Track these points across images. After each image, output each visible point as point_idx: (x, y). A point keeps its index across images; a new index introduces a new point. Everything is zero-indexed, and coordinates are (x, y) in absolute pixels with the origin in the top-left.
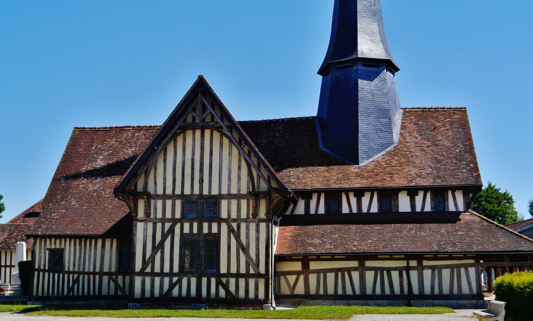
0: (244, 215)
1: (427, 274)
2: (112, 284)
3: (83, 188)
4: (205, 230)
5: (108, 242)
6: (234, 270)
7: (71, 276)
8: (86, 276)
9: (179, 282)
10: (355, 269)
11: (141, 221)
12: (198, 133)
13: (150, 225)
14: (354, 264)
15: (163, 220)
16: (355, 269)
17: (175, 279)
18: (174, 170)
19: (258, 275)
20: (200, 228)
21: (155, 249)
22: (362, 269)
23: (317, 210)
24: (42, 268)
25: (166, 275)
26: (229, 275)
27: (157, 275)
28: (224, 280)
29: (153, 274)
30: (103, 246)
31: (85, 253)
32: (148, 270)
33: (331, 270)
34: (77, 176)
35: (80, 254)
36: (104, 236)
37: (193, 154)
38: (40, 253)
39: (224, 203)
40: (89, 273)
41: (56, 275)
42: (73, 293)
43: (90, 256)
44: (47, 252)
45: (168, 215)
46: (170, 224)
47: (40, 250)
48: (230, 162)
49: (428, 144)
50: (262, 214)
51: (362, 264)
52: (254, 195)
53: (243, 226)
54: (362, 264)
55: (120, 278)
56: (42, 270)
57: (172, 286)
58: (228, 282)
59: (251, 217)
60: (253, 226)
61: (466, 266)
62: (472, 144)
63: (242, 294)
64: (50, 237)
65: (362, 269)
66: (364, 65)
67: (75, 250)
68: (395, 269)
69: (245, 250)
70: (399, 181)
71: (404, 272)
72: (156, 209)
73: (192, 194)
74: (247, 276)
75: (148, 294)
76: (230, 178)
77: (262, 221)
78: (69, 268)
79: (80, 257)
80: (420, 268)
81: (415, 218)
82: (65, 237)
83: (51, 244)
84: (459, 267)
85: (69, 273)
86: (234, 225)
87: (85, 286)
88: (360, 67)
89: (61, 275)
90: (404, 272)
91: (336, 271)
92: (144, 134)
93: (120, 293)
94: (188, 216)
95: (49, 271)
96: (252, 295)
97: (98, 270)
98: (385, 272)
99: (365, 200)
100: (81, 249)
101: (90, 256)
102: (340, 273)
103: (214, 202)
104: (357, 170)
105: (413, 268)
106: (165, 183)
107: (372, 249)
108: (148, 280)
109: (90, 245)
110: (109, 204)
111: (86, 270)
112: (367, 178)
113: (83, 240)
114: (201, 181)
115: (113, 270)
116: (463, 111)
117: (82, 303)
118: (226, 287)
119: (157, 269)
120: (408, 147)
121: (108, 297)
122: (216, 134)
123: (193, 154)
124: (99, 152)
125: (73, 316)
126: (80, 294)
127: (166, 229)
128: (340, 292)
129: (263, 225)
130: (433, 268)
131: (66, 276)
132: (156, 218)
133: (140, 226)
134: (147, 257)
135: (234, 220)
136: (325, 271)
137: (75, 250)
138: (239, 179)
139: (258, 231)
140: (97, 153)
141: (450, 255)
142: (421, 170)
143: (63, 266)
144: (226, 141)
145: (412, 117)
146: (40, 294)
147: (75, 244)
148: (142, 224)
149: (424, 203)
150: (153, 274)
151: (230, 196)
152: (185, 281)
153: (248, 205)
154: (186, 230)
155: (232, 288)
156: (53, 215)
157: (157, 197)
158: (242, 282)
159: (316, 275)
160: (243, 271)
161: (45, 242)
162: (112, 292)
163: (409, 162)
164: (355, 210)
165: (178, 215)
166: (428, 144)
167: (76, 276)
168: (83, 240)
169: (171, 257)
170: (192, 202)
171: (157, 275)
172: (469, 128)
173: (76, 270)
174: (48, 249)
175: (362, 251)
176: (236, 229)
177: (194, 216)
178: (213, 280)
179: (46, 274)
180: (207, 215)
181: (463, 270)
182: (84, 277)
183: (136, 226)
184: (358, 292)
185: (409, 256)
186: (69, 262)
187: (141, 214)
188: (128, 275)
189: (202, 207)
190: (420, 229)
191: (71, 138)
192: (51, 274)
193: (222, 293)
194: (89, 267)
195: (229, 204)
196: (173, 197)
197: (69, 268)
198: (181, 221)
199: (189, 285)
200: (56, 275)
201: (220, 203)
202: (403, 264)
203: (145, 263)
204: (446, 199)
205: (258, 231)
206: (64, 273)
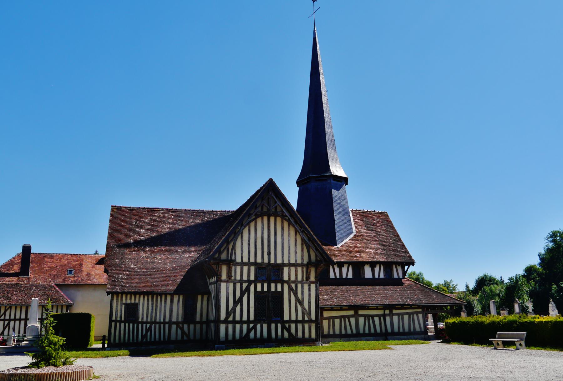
0: (299, 278)
1: (395, 318)
3: (136, 254)
4: (273, 289)
6: (293, 318)
7: (144, 325)
8: (157, 326)
9: (255, 327)
10: (352, 316)
11: (224, 282)
12: (266, 219)
13: (231, 285)
14: (352, 313)
15: (242, 281)
16: (352, 316)
17: (251, 325)
18: (249, 244)
19: (310, 321)
20: (269, 287)
21: (236, 303)
22: (356, 316)
23: (379, 276)
24: (119, 319)
25: (245, 322)
26: (290, 321)
27: (238, 322)
28: (287, 325)
29: (234, 322)
30: (172, 301)
31: (156, 307)
32: (231, 319)
33: (337, 317)
34: (128, 245)
35: (152, 307)
36: (172, 295)
37: (263, 234)
38: (117, 307)
39: (286, 270)
40: (160, 323)
41: (131, 325)
42: (147, 339)
43: (160, 309)
44: (123, 306)
45: (245, 278)
46: (247, 284)
47: (117, 304)
48: (289, 240)
49: (374, 234)
50: (312, 278)
51: (356, 313)
52: (308, 266)
53: (299, 286)
54: (356, 313)
55: (186, 326)
56: (118, 321)
57: (249, 331)
58: (290, 326)
59: (305, 279)
60: (306, 286)
62: (398, 235)
63: (300, 335)
64: (131, 293)
65: (356, 316)
66: (334, 180)
67: (148, 304)
68: (376, 316)
69: (301, 303)
70: (366, 258)
71: (382, 318)
72: (235, 272)
73: (263, 262)
74: (303, 322)
75: (230, 337)
76: (289, 252)
77: (312, 282)
78: (143, 319)
79: (152, 309)
80: (391, 315)
81: (374, 282)
82: (140, 294)
83: (126, 300)
84: (413, 313)
85: (142, 323)
86: (293, 285)
87: (156, 333)
88: (332, 181)
89: (136, 325)
90: (382, 318)
91: (340, 317)
92: (173, 215)
93: (185, 338)
94: (259, 279)
95: (125, 322)
96: (307, 335)
97: (167, 320)
98: (370, 318)
99: (344, 270)
100: (153, 304)
101: (160, 309)
102: (343, 319)
103: (279, 268)
104: (337, 249)
105: (388, 315)
106: (242, 254)
107: (365, 303)
108: (230, 327)
109: (161, 300)
110: (164, 268)
111: (158, 320)
112: (346, 255)
113: (155, 296)
114: (269, 254)
115: (180, 319)
116: (113, 208)
117: (155, 347)
118: (289, 330)
119: (238, 318)
120: (362, 235)
121: (176, 342)
122: (279, 220)
123: (263, 234)
124: (140, 227)
125: (203, 356)
126: (153, 340)
127: (244, 288)
128: (343, 332)
129: (313, 286)
130: (398, 315)
131: (140, 326)
132: (235, 279)
133: (223, 285)
134: (230, 309)
135: (293, 282)
136: (334, 318)
138: (296, 253)
139: (309, 290)
140: (138, 228)
141: (411, 306)
142: (372, 252)
144: (286, 224)
145: (358, 216)
147: (148, 299)
148: (225, 284)
149: (380, 273)
151: (290, 265)
152: (259, 326)
153: (303, 272)
154: (259, 288)
155: (293, 331)
156: (120, 276)
157: (238, 264)
158: (300, 326)
159: (327, 321)
160: (300, 318)
162: (179, 337)
163: (368, 246)
164: (338, 277)
165: (252, 278)
166: (374, 234)
167: (148, 325)
168: (155, 296)
169: (248, 309)
170: (263, 268)
171: (238, 322)
172: (393, 225)
173: (149, 320)
174: (124, 304)
175: (359, 304)
176: (294, 288)
177: (264, 278)
178: (279, 325)
179: (123, 324)
180: (273, 278)
181: (415, 316)
183: (220, 285)
184: (354, 332)
185: (385, 307)
186: (143, 314)
187: (224, 276)
188: (192, 324)
189: (270, 272)
190: (385, 290)
191: (111, 214)
192: (127, 325)
193: (286, 334)
194: (159, 318)
195: (289, 270)
196: (249, 264)
197: (143, 319)
198: (255, 282)
199: (262, 329)
200: (131, 325)
201: (282, 270)
202: (380, 312)
203: (228, 314)
204: (392, 270)
205: (309, 290)
206: (138, 323)
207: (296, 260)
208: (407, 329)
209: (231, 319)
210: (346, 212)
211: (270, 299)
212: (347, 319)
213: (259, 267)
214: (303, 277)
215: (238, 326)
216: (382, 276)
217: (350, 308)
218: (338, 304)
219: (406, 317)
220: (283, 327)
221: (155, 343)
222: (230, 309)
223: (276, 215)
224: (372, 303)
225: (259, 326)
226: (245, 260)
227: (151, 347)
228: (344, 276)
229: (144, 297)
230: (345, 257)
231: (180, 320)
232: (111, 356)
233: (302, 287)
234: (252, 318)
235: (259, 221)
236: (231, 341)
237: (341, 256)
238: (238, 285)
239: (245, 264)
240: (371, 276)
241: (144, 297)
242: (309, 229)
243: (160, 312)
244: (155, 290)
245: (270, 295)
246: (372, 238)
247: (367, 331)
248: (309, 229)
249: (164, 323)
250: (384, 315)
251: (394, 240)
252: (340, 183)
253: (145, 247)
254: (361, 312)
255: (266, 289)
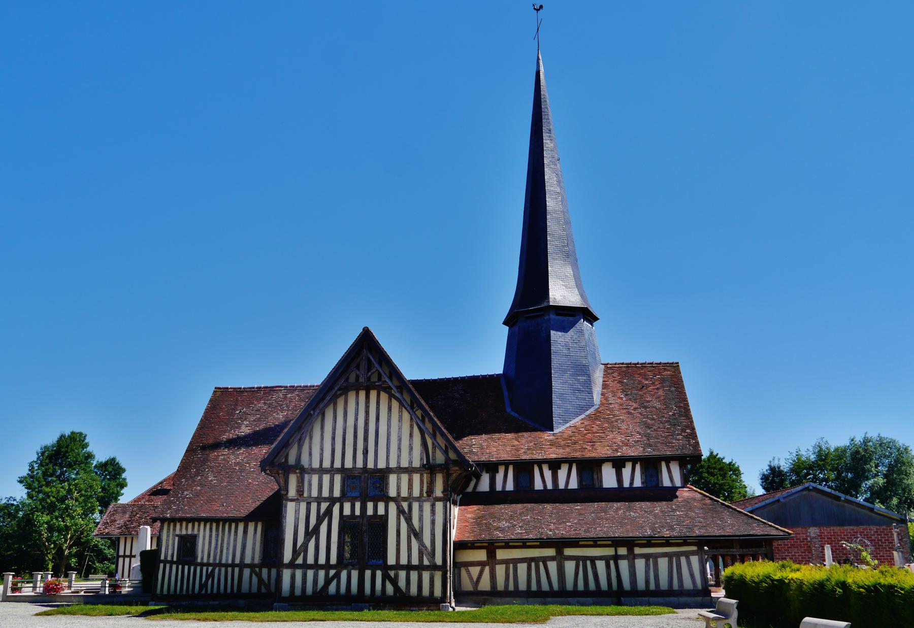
0: (416, 493)
1: (640, 564)
2: (255, 578)
3: (224, 460)
4: (370, 512)
5: (251, 526)
6: (404, 561)
7: (205, 568)
8: (223, 569)
9: (337, 576)
10: (552, 559)
11: (292, 500)
12: (362, 394)
13: (303, 505)
14: (551, 552)
15: (319, 500)
16: (552, 559)
18: (333, 438)
19: (433, 567)
20: (364, 509)
21: (308, 534)
22: (560, 558)
25: (322, 567)
26: (398, 567)
27: (310, 567)
28: (392, 573)
29: (305, 566)
30: (245, 532)
31: (223, 540)
32: (300, 561)
33: (522, 560)
34: (216, 446)
35: (217, 541)
36: (246, 520)
37: (356, 420)
38: (167, 540)
39: (393, 478)
40: (226, 566)
41: (186, 567)
43: (228, 544)
44: (177, 539)
47: (168, 536)
48: (400, 429)
49: (635, 405)
51: (560, 552)
52: (429, 468)
53: (416, 505)
54: (560, 552)
55: (265, 571)
57: (328, 581)
58: (397, 576)
59: (425, 495)
60: (427, 506)
61: (687, 555)
63: (414, 590)
64: (181, 520)
65: (560, 558)
66: (557, 314)
67: (211, 536)
68: (600, 558)
70: (602, 451)
71: (612, 562)
72: (310, 485)
73: (354, 468)
74: (420, 568)
75: (298, 592)
76: (399, 449)
78: (202, 559)
79: (217, 544)
81: (622, 495)
82: (200, 520)
83: (181, 529)
84: (678, 555)
85: (202, 565)
86: (405, 505)
87: (221, 581)
88: (552, 316)
90: (612, 562)
91: (529, 561)
94: (349, 494)
96: (426, 592)
98: (588, 562)
100: (217, 535)
101: (228, 544)
102: (533, 564)
103: (381, 476)
104: (551, 437)
105: (623, 557)
108: (299, 573)
110: (254, 479)
111: (224, 561)
112: (564, 447)
114: (365, 452)
115: (257, 560)
118: (394, 582)
119: (311, 560)
120: (612, 410)
121: (249, 595)
122: (384, 396)
123: (356, 420)
125: (206, 620)
126: (215, 591)
127: (322, 511)
129: (439, 506)
130: (647, 557)
131: (198, 568)
132: (310, 497)
133: (290, 507)
134: (299, 544)
135: (405, 499)
136: (516, 562)
137: (211, 536)
138: (411, 449)
139: (433, 512)
140: (241, 418)
141: (595, 542)
143: (195, 557)
144: (395, 404)
145: (616, 374)
146: (165, 592)
148: (293, 504)
149: (633, 477)
150: (305, 566)
151: (400, 470)
152: (344, 574)
154: (347, 511)
155: (402, 583)
157: (313, 471)
158: (414, 575)
160: (415, 561)
161: (175, 526)
162: (255, 589)
165: (337, 493)
166: (635, 405)
167: (210, 569)
169: (328, 545)
170: (354, 477)
171: (310, 567)
174: (177, 536)
175: (560, 536)
178: (379, 573)
179: (174, 567)
182: (220, 571)
183: (286, 507)
184: (556, 586)
185: (616, 543)
186: (203, 552)
189: (367, 483)
190: (629, 509)
191: (211, 400)
192: (180, 567)
193: (390, 589)
194: (227, 558)
195: (399, 479)
196: (332, 471)
197: (202, 559)
198: (341, 500)
199: (349, 580)
200: (186, 567)
201: (388, 478)
202: (610, 552)
204: (658, 472)
205: (433, 512)
207: (411, 462)
208: (523, 586)
209: (300, 561)
210: (582, 371)
211: (364, 528)
212: (541, 564)
213: (348, 475)
214: (421, 490)
215: (310, 573)
216: (638, 483)
217: (544, 543)
218: (519, 537)
219: (663, 563)
220: (385, 577)
221: (212, 597)
222: (299, 544)
223: (379, 389)
224: (588, 535)
225: (344, 574)
226: (327, 464)
227: (211, 603)
228: (562, 486)
229: (205, 526)
230: (561, 451)
231: (257, 561)
232: (116, 614)
233: (421, 507)
234: (333, 560)
235: (352, 396)
236: (310, 596)
237: (554, 449)
238: (314, 506)
239: (326, 471)
240: (614, 484)
241: (205, 526)
242: (427, 408)
243: (228, 549)
244: (219, 515)
245: (365, 521)
246: (630, 413)
247: (581, 587)
248: (427, 408)
249: (233, 565)
250: (616, 558)
251: (674, 414)
252: (571, 319)
253: (239, 448)
254: (568, 552)
255: (358, 513)
